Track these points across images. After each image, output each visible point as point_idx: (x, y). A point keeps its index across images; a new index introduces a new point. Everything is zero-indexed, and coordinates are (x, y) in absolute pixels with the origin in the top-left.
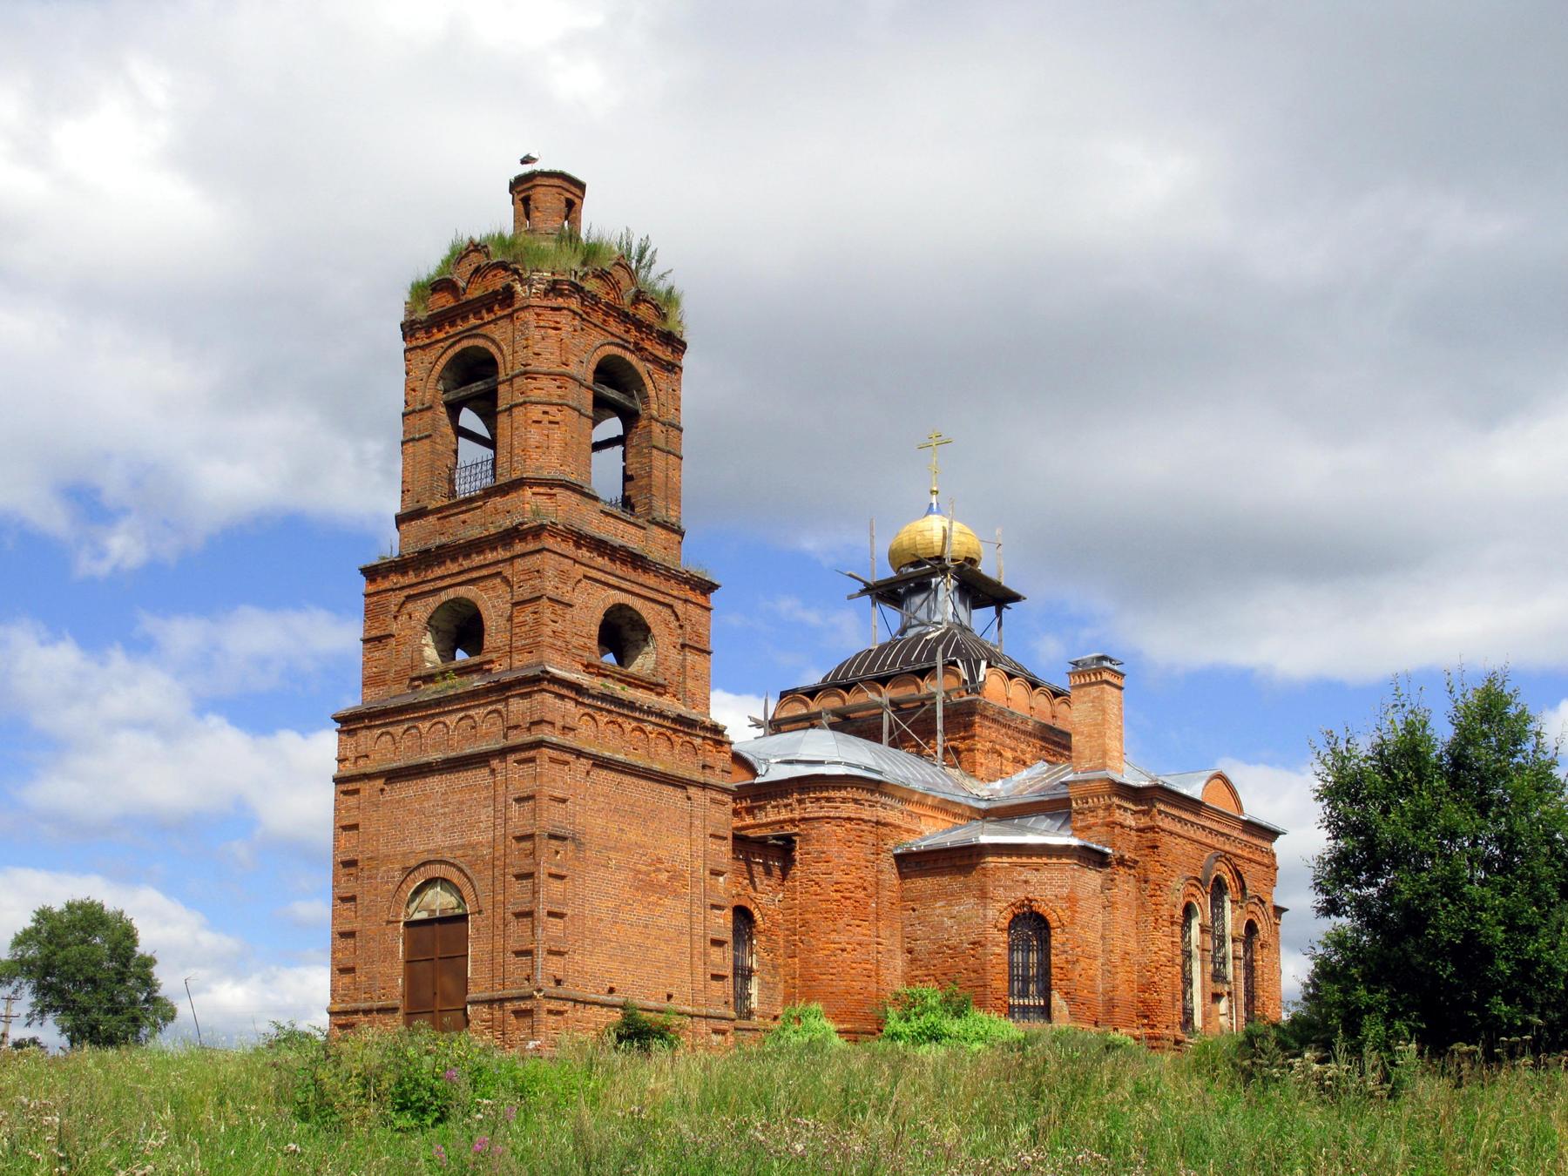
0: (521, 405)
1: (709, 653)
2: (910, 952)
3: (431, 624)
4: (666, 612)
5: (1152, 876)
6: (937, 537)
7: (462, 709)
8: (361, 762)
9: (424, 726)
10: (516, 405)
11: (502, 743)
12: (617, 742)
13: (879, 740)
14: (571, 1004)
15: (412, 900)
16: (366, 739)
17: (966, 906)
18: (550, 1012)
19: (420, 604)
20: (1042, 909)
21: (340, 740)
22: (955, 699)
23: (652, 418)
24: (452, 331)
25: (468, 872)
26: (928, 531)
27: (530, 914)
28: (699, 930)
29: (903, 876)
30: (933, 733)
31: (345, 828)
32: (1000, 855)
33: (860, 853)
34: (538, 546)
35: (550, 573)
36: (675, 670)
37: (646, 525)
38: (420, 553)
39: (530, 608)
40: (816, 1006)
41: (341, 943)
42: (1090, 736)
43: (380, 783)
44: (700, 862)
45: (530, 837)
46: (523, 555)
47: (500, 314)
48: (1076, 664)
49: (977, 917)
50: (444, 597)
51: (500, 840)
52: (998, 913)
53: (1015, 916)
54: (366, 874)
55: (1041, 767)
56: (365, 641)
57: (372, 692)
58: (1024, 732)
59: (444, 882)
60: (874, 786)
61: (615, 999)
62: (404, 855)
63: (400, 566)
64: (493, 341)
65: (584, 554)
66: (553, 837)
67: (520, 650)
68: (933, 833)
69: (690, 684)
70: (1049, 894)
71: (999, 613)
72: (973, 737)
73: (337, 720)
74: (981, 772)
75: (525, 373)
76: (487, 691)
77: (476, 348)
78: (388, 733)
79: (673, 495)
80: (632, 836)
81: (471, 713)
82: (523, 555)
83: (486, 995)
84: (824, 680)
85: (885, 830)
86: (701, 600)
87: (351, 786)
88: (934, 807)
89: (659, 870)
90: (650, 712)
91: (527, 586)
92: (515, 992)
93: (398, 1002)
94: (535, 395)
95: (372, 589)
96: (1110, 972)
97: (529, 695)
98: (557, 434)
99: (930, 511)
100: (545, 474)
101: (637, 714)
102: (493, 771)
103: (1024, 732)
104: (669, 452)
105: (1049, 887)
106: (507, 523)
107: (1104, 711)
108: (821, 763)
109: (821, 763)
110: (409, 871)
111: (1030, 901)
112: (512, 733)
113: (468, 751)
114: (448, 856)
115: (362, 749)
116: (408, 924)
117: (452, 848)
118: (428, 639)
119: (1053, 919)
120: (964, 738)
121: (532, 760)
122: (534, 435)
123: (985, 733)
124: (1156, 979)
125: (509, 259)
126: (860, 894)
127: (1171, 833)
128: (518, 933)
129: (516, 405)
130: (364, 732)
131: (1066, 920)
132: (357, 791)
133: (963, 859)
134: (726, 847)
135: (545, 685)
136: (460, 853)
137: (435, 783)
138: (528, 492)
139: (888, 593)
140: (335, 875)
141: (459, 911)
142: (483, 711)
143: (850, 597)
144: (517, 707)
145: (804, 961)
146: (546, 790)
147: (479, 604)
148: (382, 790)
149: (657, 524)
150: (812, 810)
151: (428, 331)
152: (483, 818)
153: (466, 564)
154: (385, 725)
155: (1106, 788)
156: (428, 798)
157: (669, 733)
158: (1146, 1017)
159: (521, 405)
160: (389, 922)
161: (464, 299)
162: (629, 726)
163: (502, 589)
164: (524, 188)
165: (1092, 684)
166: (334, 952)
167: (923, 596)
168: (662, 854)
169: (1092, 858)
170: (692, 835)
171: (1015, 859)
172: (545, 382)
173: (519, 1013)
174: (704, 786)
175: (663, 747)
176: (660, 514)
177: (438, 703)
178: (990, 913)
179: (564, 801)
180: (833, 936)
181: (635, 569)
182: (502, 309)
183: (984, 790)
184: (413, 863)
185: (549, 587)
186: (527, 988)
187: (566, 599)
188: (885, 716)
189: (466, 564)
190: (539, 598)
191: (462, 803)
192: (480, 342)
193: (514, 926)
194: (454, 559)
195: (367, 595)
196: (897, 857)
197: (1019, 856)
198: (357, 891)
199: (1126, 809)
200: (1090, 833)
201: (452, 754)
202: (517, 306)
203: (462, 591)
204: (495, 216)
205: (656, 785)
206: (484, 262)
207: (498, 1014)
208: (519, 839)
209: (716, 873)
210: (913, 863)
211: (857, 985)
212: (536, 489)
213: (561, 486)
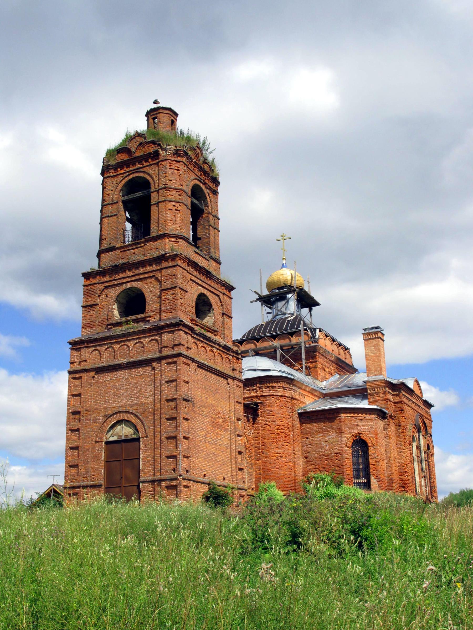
0: (163, 201)
1: (232, 318)
2: (306, 457)
3: (117, 299)
4: (217, 298)
5: (402, 423)
6: (289, 278)
7: (137, 339)
8: (83, 364)
9: (117, 347)
10: (161, 202)
11: (158, 355)
12: (204, 356)
13: (276, 360)
14: (192, 482)
15: (109, 431)
16: (85, 353)
17: (332, 436)
18: (185, 487)
19: (112, 290)
20: (365, 438)
21: (72, 353)
22: (307, 345)
24: (127, 170)
25: (140, 417)
26: (285, 275)
27: (175, 438)
28: (233, 447)
29: (301, 423)
30: (301, 359)
31: (74, 396)
32: (346, 413)
33: (286, 412)
34: (174, 264)
35: (179, 276)
36: (220, 325)
37: (209, 259)
38: (113, 266)
39: (170, 292)
40: (273, 483)
41: (70, 452)
42: (374, 361)
43: (92, 374)
44: (232, 414)
45: (175, 400)
46: (167, 268)
47: (151, 163)
48: (365, 330)
49: (338, 441)
50: (125, 287)
51: (158, 401)
52: (347, 439)
53: (354, 441)
54: (84, 418)
55: (337, 376)
56: (84, 307)
57: (87, 331)
59: (127, 422)
60: (290, 381)
61: (206, 480)
62: (105, 409)
63: (102, 273)
64: (149, 174)
65: (189, 269)
66: (185, 400)
67: (166, 311)
68: (311, 404)
69: (226, 331)
70: (367, 431)
71: (310, 311)
73: (70, 343)
74: (320, 377)
75: (165, 188)
76: (150, 330)
77: (140, 177)
78: (97, 350)
79: (217, 248)
80: (210, 401)
81: (141, 340)
82: (167, 268)
83: (151, 478)
85: (294, 401)
87: (77, 375)
88: (309, 392)
89: (219, 417)
90: (215, 343)
91: (169, 282)
92: (168, 477)
93: (102, 482)
94: (170, 198)
95: (88, 283)
96: (389, 467)
97: (173, 332)
98: (179, 215)
99: (283, 266)
100: (174, 232)
101: (211, 344)
102: (154, 368)
104: (215, 228)
105: (370, 427)
106: (156, 254)
107: (379, 350)
108: (269, 370)
109: (269, 370)
110: (108, 417)
111: (360, 434)
112: (164, 350)
113: (140, 358)
114: (129, 409)
115: (83, 357)
116: (107, 443)
117: (131, 405)
118: (115, 306)
119: (369, 442)
120: (312, 362)
121: (175, 363)
122: (170, 215)
123: (320, 360)
124: (406, 470)
125: (156, 140)
126: (287, 431)
127: (407, 404)
128: (168, 447)
129: (161, 202)
130: (84, 349)
131: (374, 442)
132: (80, 378)
133: (330, 416)
135: (181, 327)
136: (136, 407)
137: (122, 374)
138: (167, 240)
139: (267, 301)
140: (68, 418)
141: (134, 436)
142: (147, 340)
143: (252, 302)
144: (166, 337)
145: (264, 462)
146: (182, 377)
147: (144, 291)
148: (93, 377)
149: (213, 259)
150: (266, 392)
151: (116, 170)
152: (148, 390)
153: (136, 272)
154: (96, 346)
155: (383, 384)
156: (118, 381)
157: (221, 353)
158: (404, 487)
159: (163, 201)
160: (96, 442)
161: (134, 156)
162: (209, 348)
163: (155, 283)
164: (152, 114)
165: (373, 339)
166: (67, 457)
168: (220, 409)
169: (381, 414)
170: (226, 401)
171: (352, 415)
172: (173, 192)
173: (169, 487)
175: (219, 359)
177: (124, 335)
178: (344, 439)
179: (188, 382)
180: (277, 450)
181: (207, 278)
182: (152, 160)
183: (324, 384)
184: (110, 412)
185: (179, 282)
186: (174, 475)
187: (185, 289)
188: (278, 352)
189: (136, 272)
190: (175, 287)
191: (137, 383)
192: (142, 175)
193: (166, 444)
194: (130, 270)
195: (85, 286)
197: (354, 413)
198: (80, 426)
199: (390, 393)
201: (132, 360)
202: (160, 159)
203: (134, 284)
204: (141, 125)
205: (217, 377)
206: (144, 141)
207: (157, 488)
208: (168, 401)
209: (239, 420)
210: (306, 417)
211: (288, 473)
212: (170, 239)
213: (181, 238)
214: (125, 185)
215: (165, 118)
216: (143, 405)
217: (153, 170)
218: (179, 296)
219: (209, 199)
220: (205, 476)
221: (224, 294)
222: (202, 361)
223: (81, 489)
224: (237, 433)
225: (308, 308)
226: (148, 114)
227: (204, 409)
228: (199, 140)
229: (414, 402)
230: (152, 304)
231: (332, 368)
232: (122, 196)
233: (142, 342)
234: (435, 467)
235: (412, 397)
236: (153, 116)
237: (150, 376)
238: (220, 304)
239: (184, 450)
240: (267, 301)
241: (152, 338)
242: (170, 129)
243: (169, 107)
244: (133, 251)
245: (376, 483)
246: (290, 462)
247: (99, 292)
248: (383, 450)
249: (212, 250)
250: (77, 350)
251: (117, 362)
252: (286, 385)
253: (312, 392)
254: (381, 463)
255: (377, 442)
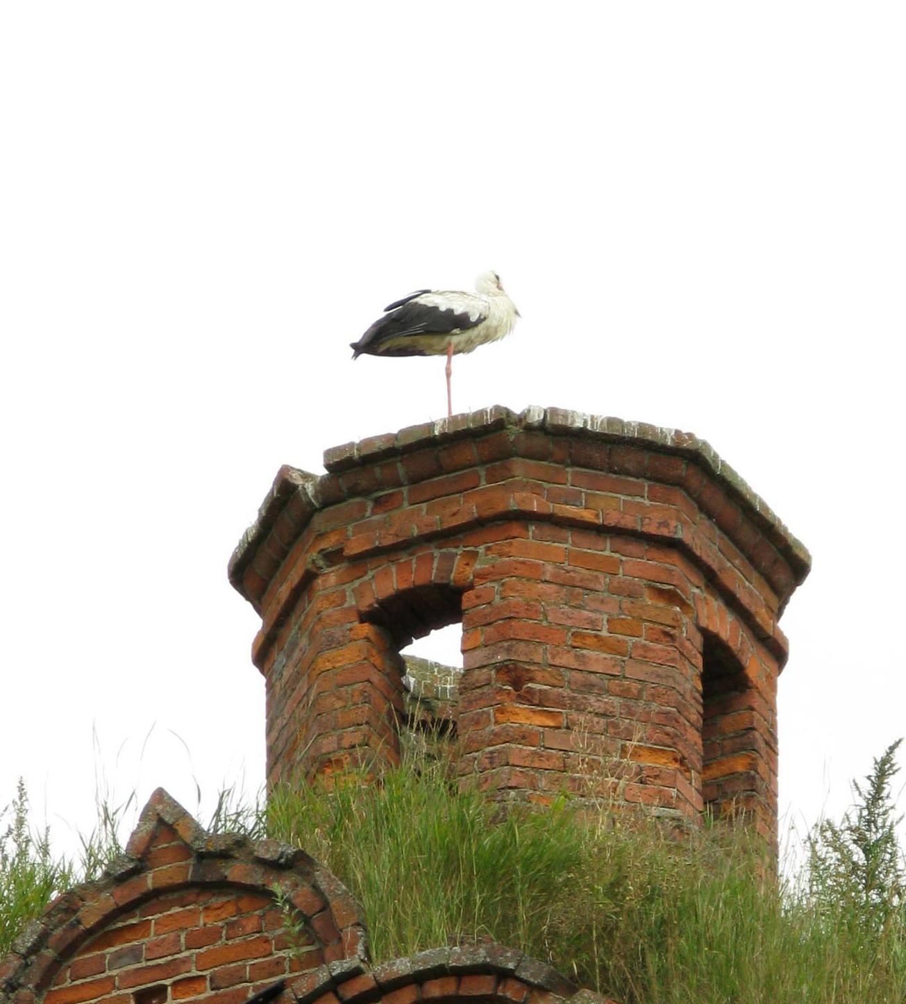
204: (194, 727)
215: (599, 615)
226: (281, 553)
234: (776, 514)
236: (388, 582)
242: (689, 788)
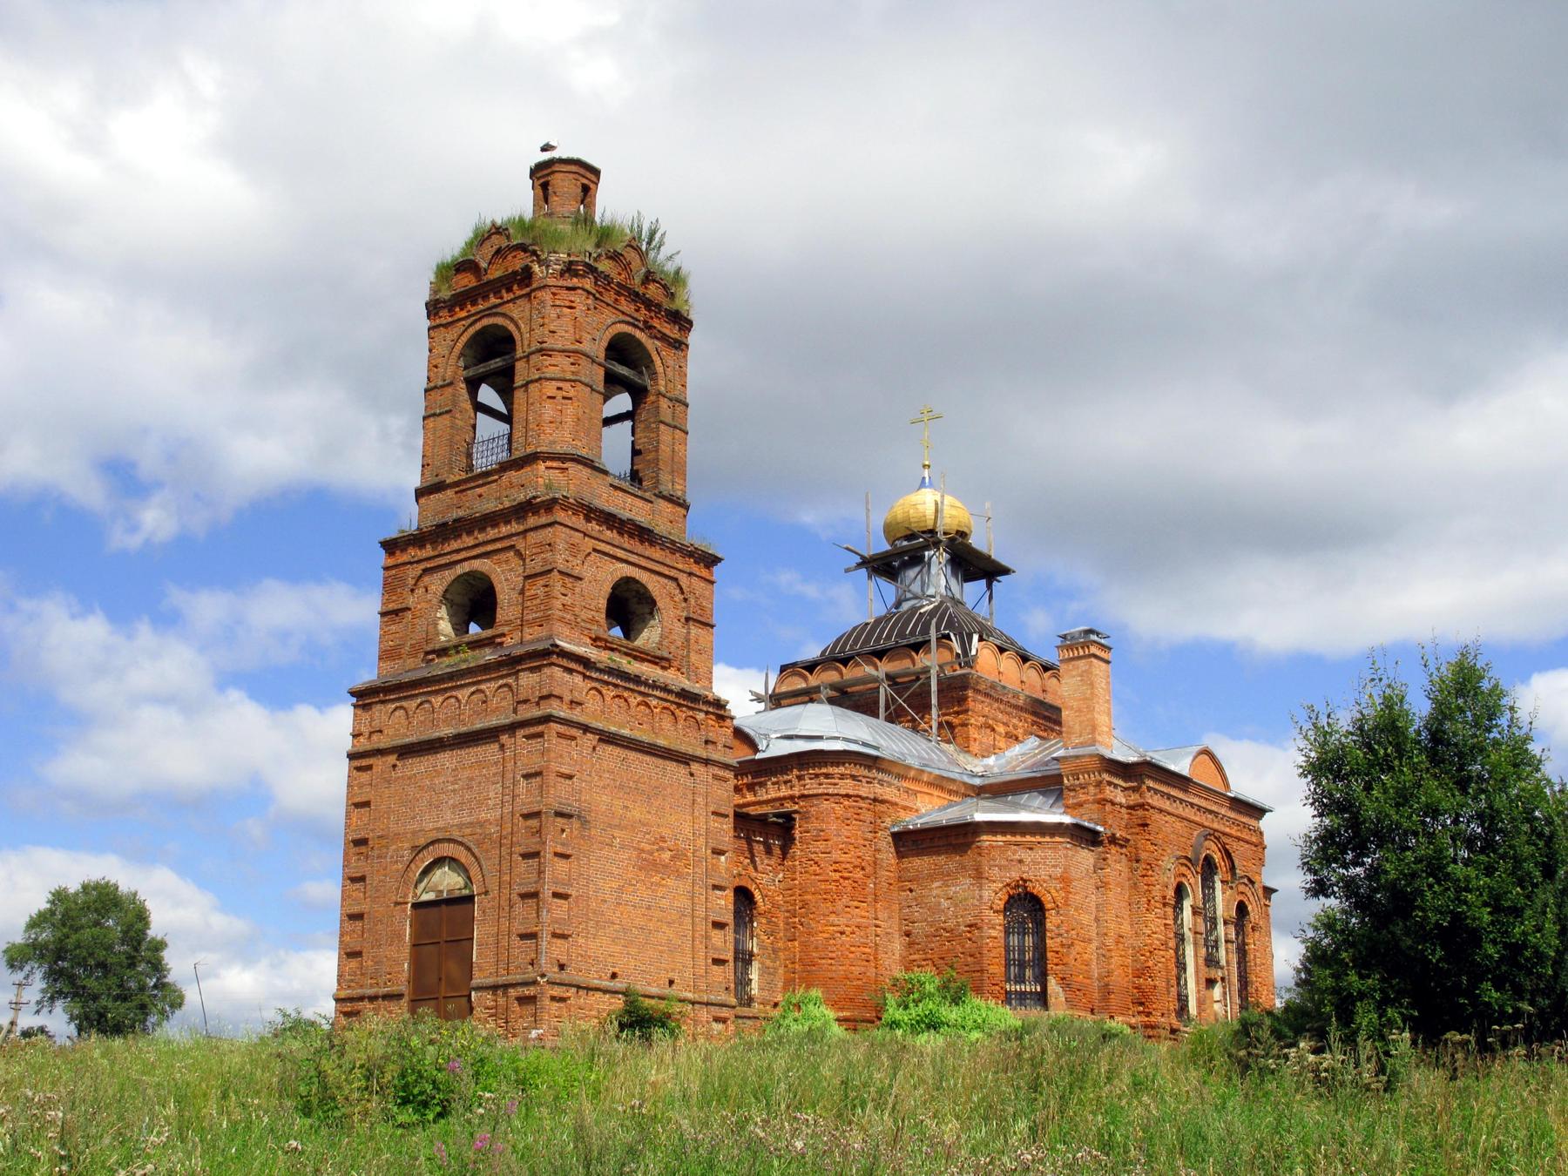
2: (908, 934)
3: (447, 597)
4: (671, 585)
5: (1144, 855)
6: (930, 511)
8: (375, 737)
9: (437, 700)
11: (512, 718)
14: (574, 990)
15: (420, 880)
16: (380, 713)
17: (962, 886)
18: (553, 998)
19: (437, 576)
20: (1037, 889)
22: (949, 673)
23: (659, 394)
24: (473, 310)
25: (476, 850)
28: (701, 912)
29: (900, 855)
31: (358, 805)
32: (995, 833)
33: (858, 831)
34: (550, 519)
35: (561, 546)
39: (541, 582)
40: (816, 993)
41: (349, 926)
42: (1079, 710)
43: (392, 759)
45: (537, 814)
46: (536, 528)
47: (519, 293)
48: (1064, 637)
49: (972, 898)
50: (460, 570)
51: (508, 818)
52: (993, 894)
53: (1010, 897)
55: (1032, 742)
56: (383, 614)
58: (1016, 707)
59: (452, 861)
60: (871, 761)
61: (618, 984)
62: (414, 833)
64: (512, 319)
65: (593, 527)
66: (559, 814)
67: (531, 623)
68: (929, 811)
69: (694, 658)
70: (1043, 874)
71: (989, 586)
72: (966, 711)
73: (353, 694)
74: (975, 747)
75: (541, 350)
76: (498, 665)
78: (402, 707)
79: (679, 470)
80: (636, 814)
81: (483, 687)
82: (536, 528)
83: (491, 981)
84: (823, 653)
85: (882, 808)
86: (704, 573)
87: (364, 762)
88: (930, 784)
89: (661, 849)
90: (654, 686)
91: (538, 559)
92: (519, 978)
93: (403, 988)
94: (551, 372)
95: (391, 562)
96: (1105, 957)
97: (538, 669)
98: (570, 409)
99: (923, 484)
100: (558, 449)
101: (642, 689)
103: (1016, 707)
105: (1045, 867)
107: (1092, 684)
108: (820, 738)
109: (820, 738)
110: (418, 850)
112: (521, 707)
113: (478, 726)
114: (456, 834)
116: (415, 906)
117: (460, 826)
118: (443, 612)
120: (958, 713)
121: (540, 735)
122: (549, 411)
123: (979, 708)
124: (1150, 964)
125: (528, 242)
126: (859, 874)
127: (1161, 811)
130: (379, 707)
132: (369, 768)
134: (728, 825)
136: (468, 831)
137: (446, 759)
138: (541, 466)
139: (883, 567)
141: (466, 892)
142: (494, 685)
143: (847, 571)
144: (527, 681)
146: (554, 766)
148: (394, 766)
149: (664, 498)
150: (811, 787)
152: (492, 795)
153: (481, 537)
157: (673, 707)
158: (1142, 1004)
160: (397, 904)
161: (485, 279)
162: (635, 700)
163: (516, 562)
164: (543, 174)
165: (1080, 658)
166: (342, 935)
167: (917, 569)
168: (666, 832)
169: (1085, 836)
170: (693, 813)
171: (1009, 838)
172: (560, 359)
173: (522, 1000)
174: (707, 762)
176: (666, 488)
177: (451, 676)
178: (986, 894)
179: (570, 777)
180: (832, 918)
181: (642, 542)
183: (977, 766)
184: (422, 842)
186: (531, 973)
187: (575, 573)
188: (882, 691)
189: (481, 537)
190: (550, 571)
191: (471, 779)
192: (499, 321)
194: (470, 533)
195: (386, 569)
196: (894, 835)
197: (1014, 834)
199: (1116, 786)
200: (1082, 811)
201: (463, 729)
202: (534, 286)
203: (477, 565)
204: (518, 201)
208: (526, 816)
209: (718, 852)
210: (911, 842)
211: (856, 970)
212: (549, 464)
214: (468, 345)
216: (481, 824)
217: (518, 311)
218: (558, 588)
219: (658, 362)
220: (614, 976)
221: (690, 574)
222: (613, 729)
223: (366, 1003)
224: (711, 882)
225: (984, 582)
227: (617, 833)
228: (640, 228)
229: (1192, 805)
230: (507, 608)
231: (1020, 724)
232: (466, 368)
233: (482, 691)
235: (1186, 791)
237: (496, 763)
238: (679, 597)
239: (556, 921)
240: (883, 567)
241: (501, 682)
243: (575, 156)
244: (479, 490)
245: (1062, 995)
246: (865, 945)
247: (411, 582)
248: (1086, 919)
249: (665, 477)
250: (366, 707)
251: (437, 735)
252: (863, 772)
253: (941, 783)
254: (1078, 947)
255: (1067, 899)
